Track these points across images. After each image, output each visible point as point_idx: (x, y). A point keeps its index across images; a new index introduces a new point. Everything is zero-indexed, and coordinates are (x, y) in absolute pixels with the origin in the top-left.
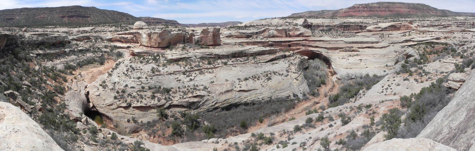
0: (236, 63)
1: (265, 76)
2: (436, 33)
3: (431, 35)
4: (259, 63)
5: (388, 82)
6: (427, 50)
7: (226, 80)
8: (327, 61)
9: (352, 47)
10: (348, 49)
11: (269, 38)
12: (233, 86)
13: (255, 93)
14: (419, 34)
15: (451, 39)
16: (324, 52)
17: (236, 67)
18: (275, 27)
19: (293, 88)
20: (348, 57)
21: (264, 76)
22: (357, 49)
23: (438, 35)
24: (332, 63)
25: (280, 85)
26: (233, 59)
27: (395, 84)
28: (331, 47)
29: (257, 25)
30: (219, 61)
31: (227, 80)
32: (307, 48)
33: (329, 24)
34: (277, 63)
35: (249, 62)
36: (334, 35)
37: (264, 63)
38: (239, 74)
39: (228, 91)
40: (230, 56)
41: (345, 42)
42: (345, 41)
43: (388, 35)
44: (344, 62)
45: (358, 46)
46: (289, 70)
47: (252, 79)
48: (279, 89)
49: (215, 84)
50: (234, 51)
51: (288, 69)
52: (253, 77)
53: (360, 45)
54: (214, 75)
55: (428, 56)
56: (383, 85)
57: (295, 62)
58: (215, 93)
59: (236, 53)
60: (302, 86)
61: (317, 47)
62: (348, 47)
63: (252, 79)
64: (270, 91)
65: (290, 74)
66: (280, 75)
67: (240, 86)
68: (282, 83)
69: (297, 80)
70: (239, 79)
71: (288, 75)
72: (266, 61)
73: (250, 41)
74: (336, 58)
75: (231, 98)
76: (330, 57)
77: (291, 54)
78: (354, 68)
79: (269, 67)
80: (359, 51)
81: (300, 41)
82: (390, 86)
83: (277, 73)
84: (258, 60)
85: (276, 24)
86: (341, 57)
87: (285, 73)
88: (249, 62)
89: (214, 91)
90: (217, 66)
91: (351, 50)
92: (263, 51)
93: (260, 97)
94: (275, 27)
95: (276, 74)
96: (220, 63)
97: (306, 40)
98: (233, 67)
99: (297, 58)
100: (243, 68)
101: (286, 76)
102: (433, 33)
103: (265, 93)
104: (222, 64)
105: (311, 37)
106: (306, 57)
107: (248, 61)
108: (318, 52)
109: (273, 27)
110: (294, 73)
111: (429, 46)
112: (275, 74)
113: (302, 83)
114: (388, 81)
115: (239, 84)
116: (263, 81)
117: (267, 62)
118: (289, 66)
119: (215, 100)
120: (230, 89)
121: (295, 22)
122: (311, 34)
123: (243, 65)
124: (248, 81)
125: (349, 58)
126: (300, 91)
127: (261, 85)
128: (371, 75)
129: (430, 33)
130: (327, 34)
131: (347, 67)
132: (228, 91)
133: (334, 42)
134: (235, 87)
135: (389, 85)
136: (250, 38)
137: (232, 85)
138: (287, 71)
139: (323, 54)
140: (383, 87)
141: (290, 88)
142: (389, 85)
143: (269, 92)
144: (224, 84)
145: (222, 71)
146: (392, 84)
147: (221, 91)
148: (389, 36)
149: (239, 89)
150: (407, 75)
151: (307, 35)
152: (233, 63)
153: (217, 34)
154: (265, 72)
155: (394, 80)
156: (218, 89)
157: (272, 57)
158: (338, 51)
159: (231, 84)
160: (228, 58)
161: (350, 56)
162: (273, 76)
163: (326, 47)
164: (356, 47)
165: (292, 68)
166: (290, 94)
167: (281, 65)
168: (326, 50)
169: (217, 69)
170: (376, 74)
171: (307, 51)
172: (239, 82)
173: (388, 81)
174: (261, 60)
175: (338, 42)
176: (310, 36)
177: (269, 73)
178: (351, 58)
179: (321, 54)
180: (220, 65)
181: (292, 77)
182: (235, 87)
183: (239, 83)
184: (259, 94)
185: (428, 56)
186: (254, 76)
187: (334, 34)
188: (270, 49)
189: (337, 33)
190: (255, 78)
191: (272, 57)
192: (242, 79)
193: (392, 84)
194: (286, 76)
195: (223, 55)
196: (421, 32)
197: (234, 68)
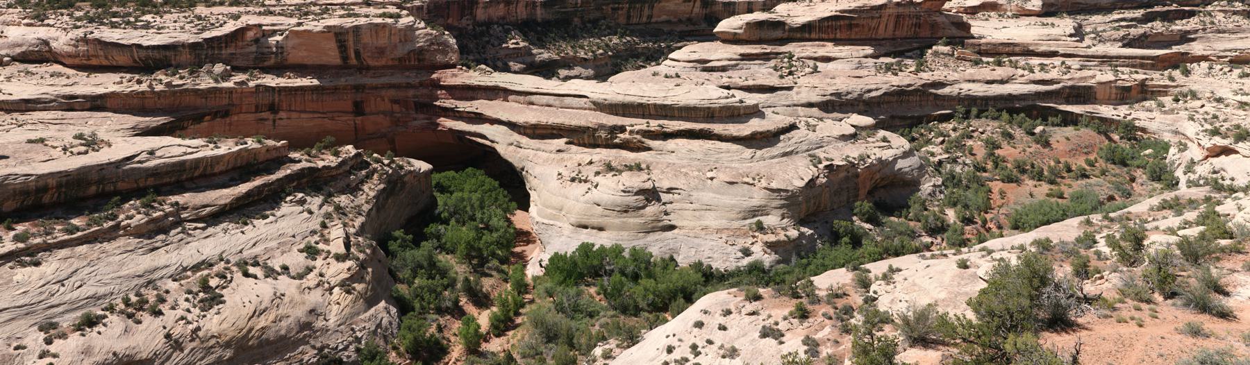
2: (1069, 61)
3: (1039, 75)
6: (1005, 151)
9: (622, 129)
14: (977, 63)
15: (1161, 105)
20: (597, 173)
21: (190, 292)
23: (1079, 74)
27: (722, 347)
42: (594, 97)
43: (811, 63)
46: (321, 246)
47: (122, 312)
51: (317, 238)
52: (127, 302)
53: (654, 124)
55: (996, 186)
56: (675, 343)
63: (122, 312)
65: (319, 262)
76: (528, 166)
80: (649, 149)
82: (697, 354)
86: (565, 173)
87: (297, 260)
91: (617, 141)
95: (252, 270)
102: (1057, 61)
108: (479, 140)
111: (1018, 133)
112: (246, 275)
114: (699, 325)
118: (324, 226)
124: (100, 328)
125: (599, 179)
128: (683, 260)
129: (1035, 61)
131: (584, 221)
133: (551, 100)
135: (694, 347)
138: (312, 252)
139: (501, 149)
140: (670, 350)
142: (694, 347)
146: (710, 342)
148: (815, 70)
150: (786, 312)
155: (723, 328)
161: (609, 168)
170: (705, 262)
173: (699, 325)
175: (568, 100)
185: (996, 186)
193: (710, 342)
196: (987, 54)
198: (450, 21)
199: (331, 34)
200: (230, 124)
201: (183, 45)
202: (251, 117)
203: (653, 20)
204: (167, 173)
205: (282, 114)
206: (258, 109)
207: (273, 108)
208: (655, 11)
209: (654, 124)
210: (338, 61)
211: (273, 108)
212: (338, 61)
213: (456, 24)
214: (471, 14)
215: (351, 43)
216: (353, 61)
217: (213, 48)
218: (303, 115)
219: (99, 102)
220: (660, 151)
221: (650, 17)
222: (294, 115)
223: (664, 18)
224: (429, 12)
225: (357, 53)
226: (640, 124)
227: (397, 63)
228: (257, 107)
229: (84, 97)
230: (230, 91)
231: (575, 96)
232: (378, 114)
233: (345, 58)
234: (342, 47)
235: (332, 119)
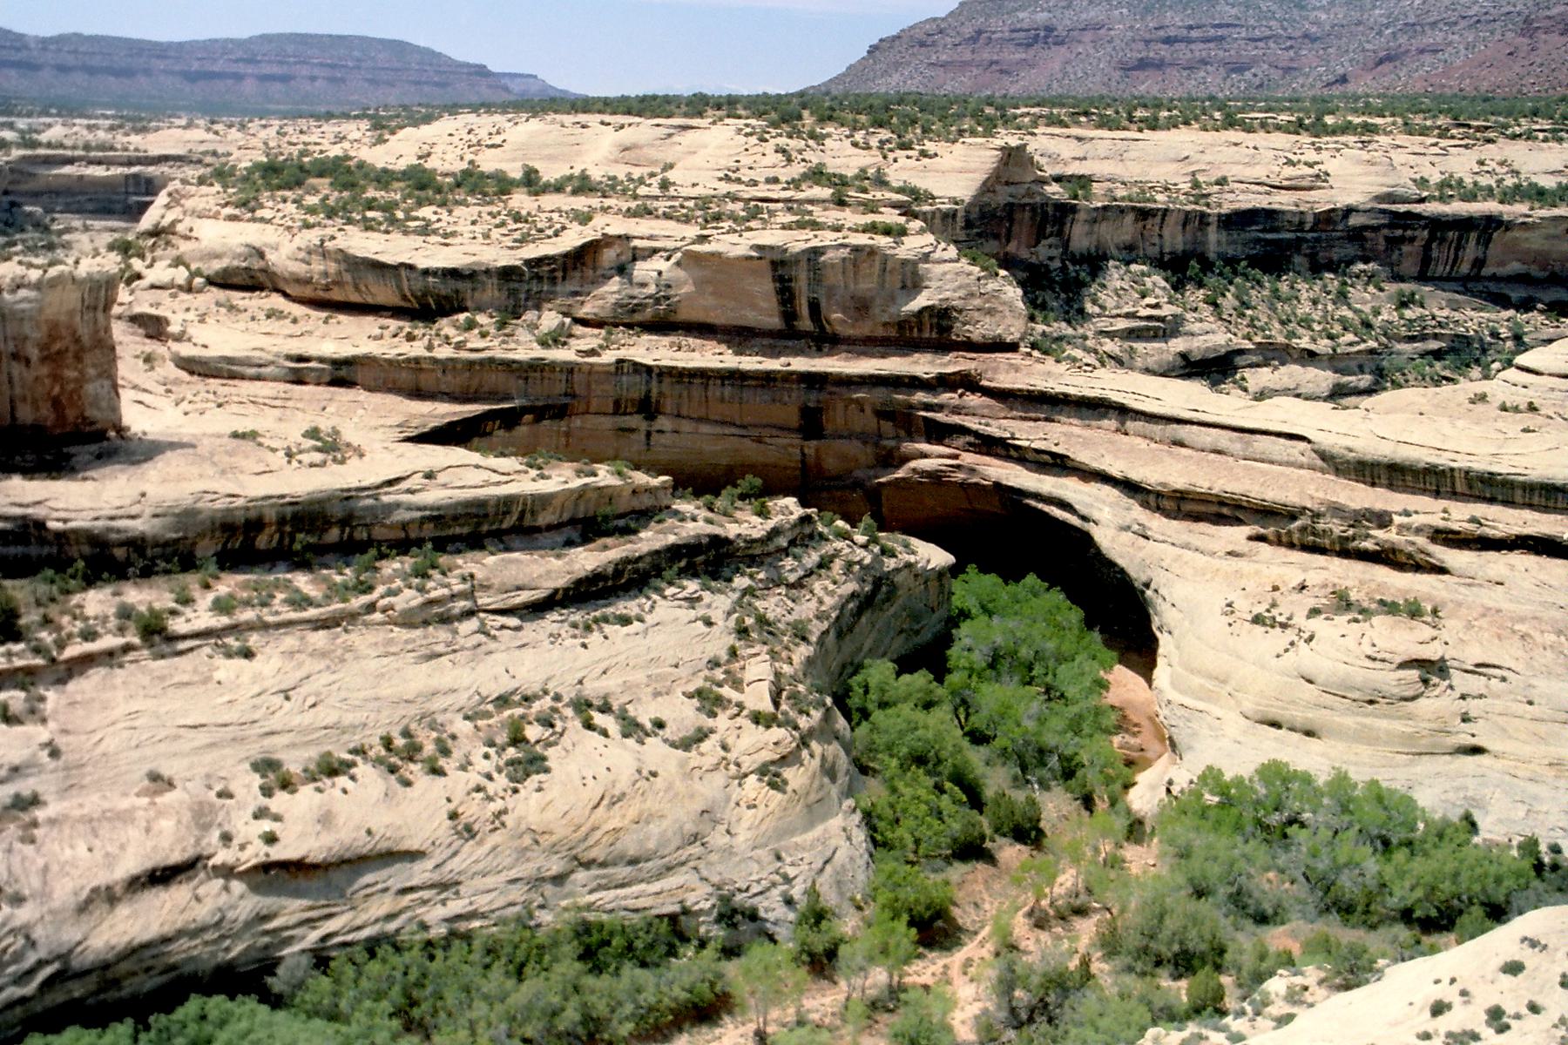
0: (248, 615)
1: (502, 738)
4: (469, 614)
5: (1507, 979)
7: (155, 777)
8: (1123, 618)
9: (1383, 520)
10: (1337, 527)
11: (620, 334)
12: (206, 827)
13: (396, 883)
16: (1111, 524)
17: (248, 654)
18: (692, 231)
19: (729, 851)
20: (1314, 612)
21: (491, 744)
22: (1421, 541)
24: (1163, 638)
25: (615, 823)
26: (228, 584)
28: (1179, 482)
29: (531, 181)
30: (96, 601)
31: (159, 782)
32: (968, 458)
33: (1261, 202)
34: (625, 621)
35: (371, 608)
36: (1306, 323)
37: (513, 621)
38: (275, 723)
39: (162, 877)
40: (206, 549)
41: (1324, 456)
42: (1326, 441)
44: (1262, 666)
45: (1437, 521)
46: (727, 691)
48: (598, 853)
49: (52, 822)
50: (240, 502)
51: (719, 674)
52: (387, 743)
53: (1460, 515)
54: (42, 733)
57: (805, 609)
58: (44, 894)
59: (254, 524)
60: (810, 836)
61: (1059, 464)
62: (1337, 510)
63: (379, 761)
64: (525, 870)
65: (722, 721)
66: (631, 728)
67: (266, 825)
68: (632, 809)
69: (777, 784)
70: (266, 766)
71: (701, 735)
72: (524, 597)
73: (443, 352)
74: (1196, 583)
75: (180, 933)
76: (1159, 579)
77: (775, 532)
78: (1340, 734)
79: (550, 657)
80: (1441, 570)
81: (914, 383)
83: (605, 709)
84: (458, 587)
85: (709, 185)
87: (682, 714)
88: (371, 608)
89: (36, 882)
90: (74, 650)
91: (1368, 545)
92: (508, 502)
93: (436, 915)
94: (692, 231)
95: (599, 719)
96: (105, 619)
97: (967, 382)
98: (220, 661)
99: (837, 566)
100: (312, 665)
101: (686, 744)
103: (480, 883)
104: (121, 630)
105: (1015, 358)
106: (934, 556)
107: (365, 599)
109: (671, 227)
110: (757, 718)
112: (589, 726)
113: (815, 811)
114: (1514, 968)
115: (260, 814)
116: (474, 778)
117: (537, 609)
119: (42, 953)
120: (176, 857)
121: (903, 170)
122: (1012, 327)
123: (319, 638)
124: (342, 781)
125: (1317, 624)
126: (788, 880)
127: (453, 816)
130: (1229, 301)
131: (1275, 713)
132: (162, 877)
133: (1223, 439)
134: (227, 838)
136: (445, 326)
137: (202, 817)
138: (709, 701)
140: (1438, 1009)
141: (695, 850)
143: (513, 874)
144: (126, 817)
145: (120, 694)
146: (1534, 1008)
147: (102, 878)
149: (257, 853)
151: (981, 330)
152: (225, 620)
153: (84, 332)
154: (503, 701)
156: (73, 863)
157: (587, 559)
158: (1236, 535)
159: (187, 816)
160: (188, 563)
162: (566, 741)
163: (1135, 476)
164: (1417, 520)
165: (748, 676)
166: (690, 899)
167: (673, 632)
168: (1137, 513)
169: (80, 686)
171: (963, 485)
172: (267, 792)
173: (1514, 968)
174: (486, 587)
175: (1262, 443)
176: (1013, 347)
177: (537, 706)
178: (1333, 631)
179: (1087, 538)
180: (108, 642)
181: (731, 756)
182: (227, 838)
183: (265, 801)
184: (426, 894)
186: (406, 733)
187: (1304, 309)
188: (577, 483)
189: (1342, 297)
190: (403, 754)
191: (587, 559)
192: (294, 764)
193: (1534, 1008)
194: (686, 744)
195: (137, 544)
197: (228, 669)
198: (1012, 248)
199: (765, 264)
200: (567, 434)
201: (487, 272)
202: (607, 422)
203: (1486, 272)
204: (455, 518)
205: (663, 422)
206: (618, 409)
207: (648, 408)
208: (1494, 250)
209: (1460, 515)
210: (774, 322)
211: (648, 408)
212: (774, 322)
213: (1024, 254)
214: (1060, 233)
215: (802, 285)
216: (806, 324)
217: (539, 278)
218: (705, 429)
219: (343, 373)
220: (1470, 580)
221: (1479, 263)
222: (686, 426)
223: (1515, 267)
224: (969, 224)
225: (814, 307)
226: (1430, 510)
227: (893, 333)
228: (617, 403)
229: (321, 360)
230: (570, 369)
231: (1279, 435)
232: (849, 437)
233: (789, 316)
234: (785, 293)
235: (759, 440)
